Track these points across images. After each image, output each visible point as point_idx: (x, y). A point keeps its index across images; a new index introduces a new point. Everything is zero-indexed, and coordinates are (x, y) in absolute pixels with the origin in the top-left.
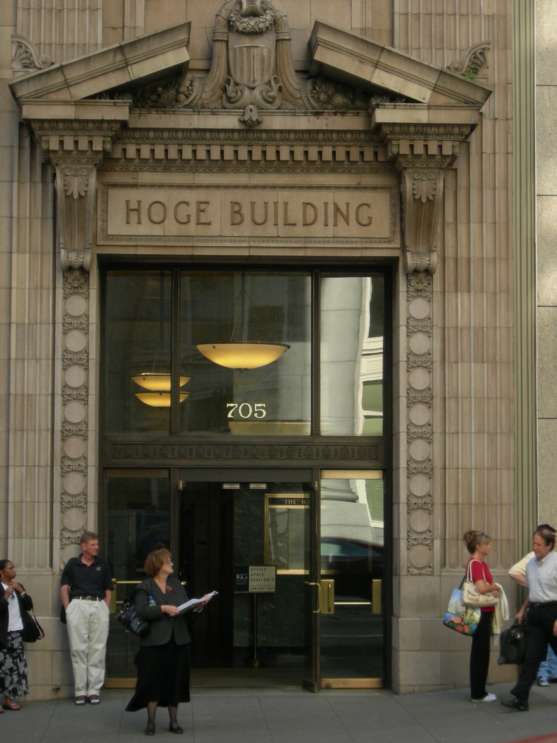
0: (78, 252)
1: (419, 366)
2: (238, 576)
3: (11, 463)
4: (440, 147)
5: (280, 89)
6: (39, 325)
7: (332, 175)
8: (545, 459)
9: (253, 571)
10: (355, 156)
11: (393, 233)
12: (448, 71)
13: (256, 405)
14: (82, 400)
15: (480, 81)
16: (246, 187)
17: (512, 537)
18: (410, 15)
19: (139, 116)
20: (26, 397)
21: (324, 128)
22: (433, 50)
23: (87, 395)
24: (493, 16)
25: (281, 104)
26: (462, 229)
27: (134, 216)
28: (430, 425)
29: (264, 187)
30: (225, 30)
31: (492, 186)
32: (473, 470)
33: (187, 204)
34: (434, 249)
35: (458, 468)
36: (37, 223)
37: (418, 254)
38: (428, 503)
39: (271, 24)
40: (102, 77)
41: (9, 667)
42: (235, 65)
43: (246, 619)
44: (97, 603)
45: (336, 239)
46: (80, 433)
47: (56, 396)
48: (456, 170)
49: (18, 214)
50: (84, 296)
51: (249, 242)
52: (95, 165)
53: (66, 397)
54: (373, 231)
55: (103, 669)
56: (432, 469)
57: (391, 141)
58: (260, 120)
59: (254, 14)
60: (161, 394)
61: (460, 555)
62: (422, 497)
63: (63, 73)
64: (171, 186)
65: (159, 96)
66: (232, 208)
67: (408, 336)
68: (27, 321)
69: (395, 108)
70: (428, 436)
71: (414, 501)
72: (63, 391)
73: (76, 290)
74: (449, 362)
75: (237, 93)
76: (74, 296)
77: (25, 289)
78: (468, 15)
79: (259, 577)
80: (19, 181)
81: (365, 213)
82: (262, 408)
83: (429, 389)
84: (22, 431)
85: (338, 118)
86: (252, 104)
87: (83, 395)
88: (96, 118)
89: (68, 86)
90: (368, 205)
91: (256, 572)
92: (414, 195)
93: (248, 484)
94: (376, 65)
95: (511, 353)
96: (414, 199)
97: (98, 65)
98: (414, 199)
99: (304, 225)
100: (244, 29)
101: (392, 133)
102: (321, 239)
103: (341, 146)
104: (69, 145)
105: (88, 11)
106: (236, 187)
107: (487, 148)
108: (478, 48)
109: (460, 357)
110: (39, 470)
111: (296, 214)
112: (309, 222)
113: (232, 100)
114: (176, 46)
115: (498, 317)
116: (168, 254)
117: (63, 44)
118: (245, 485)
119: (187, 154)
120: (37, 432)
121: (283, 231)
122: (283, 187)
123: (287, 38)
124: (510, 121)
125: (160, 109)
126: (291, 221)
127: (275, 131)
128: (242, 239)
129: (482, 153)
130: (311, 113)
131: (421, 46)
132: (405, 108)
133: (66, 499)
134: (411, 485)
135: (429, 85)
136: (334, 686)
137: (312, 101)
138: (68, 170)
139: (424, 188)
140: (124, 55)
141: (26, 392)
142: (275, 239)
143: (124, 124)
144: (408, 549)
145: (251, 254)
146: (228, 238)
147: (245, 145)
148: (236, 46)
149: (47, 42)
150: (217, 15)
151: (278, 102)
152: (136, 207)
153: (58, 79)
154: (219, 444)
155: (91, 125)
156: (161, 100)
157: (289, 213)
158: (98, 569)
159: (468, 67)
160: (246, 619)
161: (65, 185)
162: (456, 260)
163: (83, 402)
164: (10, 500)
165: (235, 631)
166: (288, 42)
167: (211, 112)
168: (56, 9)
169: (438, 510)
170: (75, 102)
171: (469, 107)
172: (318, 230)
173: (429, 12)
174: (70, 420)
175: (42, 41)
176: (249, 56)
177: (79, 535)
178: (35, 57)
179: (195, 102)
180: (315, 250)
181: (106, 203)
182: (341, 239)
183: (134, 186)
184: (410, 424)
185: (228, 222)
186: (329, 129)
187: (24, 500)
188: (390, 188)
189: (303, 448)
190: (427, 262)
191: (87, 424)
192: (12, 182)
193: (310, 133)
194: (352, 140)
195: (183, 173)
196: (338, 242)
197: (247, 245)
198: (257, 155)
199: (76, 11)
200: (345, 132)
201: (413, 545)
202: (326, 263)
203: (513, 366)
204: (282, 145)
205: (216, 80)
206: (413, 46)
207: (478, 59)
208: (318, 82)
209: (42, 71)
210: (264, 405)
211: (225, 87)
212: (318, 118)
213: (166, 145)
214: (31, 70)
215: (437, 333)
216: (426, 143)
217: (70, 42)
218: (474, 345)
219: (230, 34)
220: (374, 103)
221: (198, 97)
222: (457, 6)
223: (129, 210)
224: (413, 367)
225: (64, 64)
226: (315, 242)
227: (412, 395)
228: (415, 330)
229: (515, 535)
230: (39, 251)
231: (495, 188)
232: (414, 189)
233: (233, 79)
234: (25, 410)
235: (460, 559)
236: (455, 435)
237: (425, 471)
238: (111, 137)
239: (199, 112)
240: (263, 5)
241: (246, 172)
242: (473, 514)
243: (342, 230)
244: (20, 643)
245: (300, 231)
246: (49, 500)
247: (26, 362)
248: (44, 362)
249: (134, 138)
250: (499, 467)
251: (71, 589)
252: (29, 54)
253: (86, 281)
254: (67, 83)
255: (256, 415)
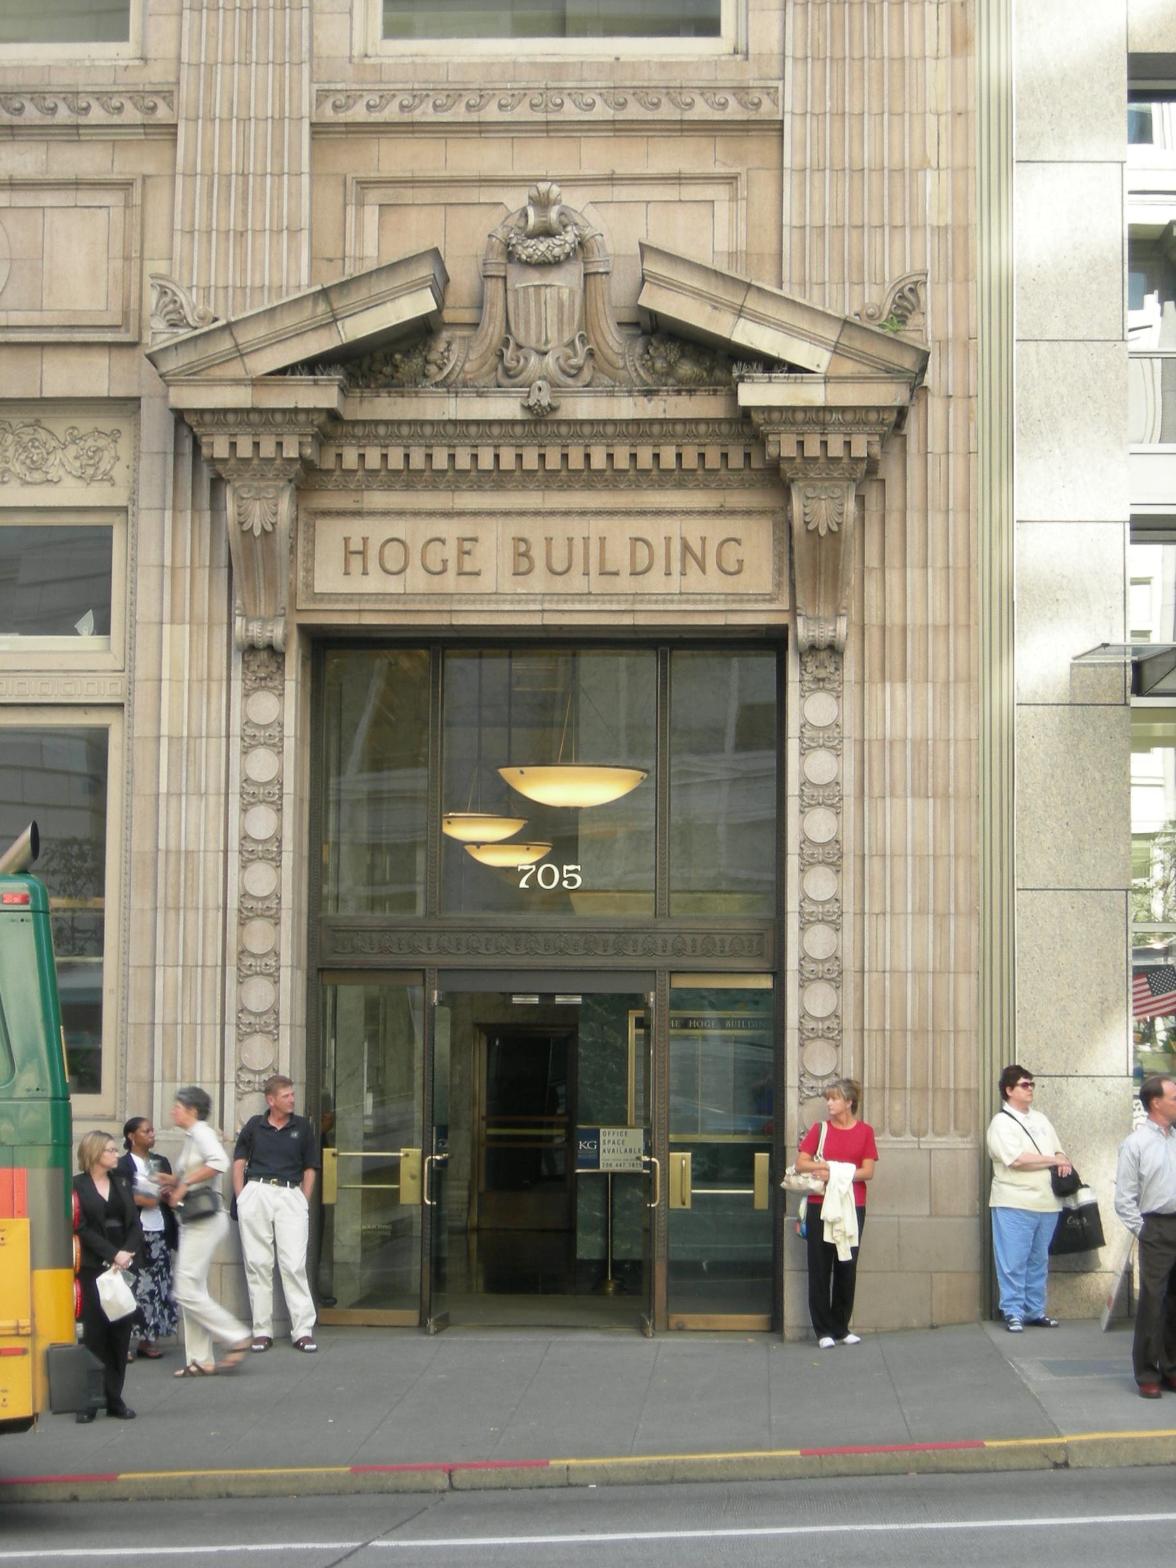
0: (265, 621)
1: (819, 804)
2: (581, 1145)
3: (159, 960)
4: (848, 444)
5: (591, 354)
6: (204, 740)
7: (676, 492)
8: (1029, 957)
9: (608, 1135)
10: (713, 460)
11: (778, 585)
12: (856, 320)
13: (565, 868)
14: (272, 859)
15: (909, 335)
16: (537, 513)
17: (973, 1085)
18: (808, 229)
19: (361, 402)
20: (183, 856)
21: (661, 416)
22: (847, 285)
23: (280, 853)
24: (946, 227)
25: (592, 378)
26: (893, 577)
27: (356, 563)
28: (837, 900)
29: (567, 513)
30: (502, 260)
31: (943, 508)
32: (909, 975)
33: (443, 541)
34: (843, 611)
35: (884, 972)
36: (203, 575)
37: (817, 619)
38: (834, 1029)
39: (574, 250)
40: (295, 340)
41: (147, 1290)
42: (517, 315)
43: (598, 1214)
44: (287, 1191)
45: (684, 597)
46: (268, 913)
47: (230, 854)
48: (883, 481)
49: (173, 561)
50: (277, 692)
51: (542, 602)
52: (290, 481)
53: (246, 855)
54: (746, 583)
55: (108, 1302)
56: (841, 973)
57: (767, 435)
58: (554, 405)
59: (547, 232)
60: (478, 847)
61: (887, 1114)
62: (823, 1019)
63: (232, 334)
64: (416, 514)
65: (396, 367)
66: (516, 547)
67: (802, 754)
68: (185, 734)
69: (770, 381)
70: (834, 918)
71: (811, 1024)
72: (242, 845)
73: (263, 683)
74: (871, 797)
75: (518, 362)
76: (260, 693)
77: (182, 681)
78: (903, 226)
79: (616, 1147)
80: (174, 508)
81: (732, 554)
82: (576, 871)
83: (837, 841)
84: (177, 909)
85: (683, 399)
86: (544, 378)
87: (272, 852)
88: (285, 406)
89: (242, 355)
90: (738, 541)
91: (611, 1138)
92: (807, 523)
93: (552, 996)
94: (740, 312)
95: (973, 780)
96: (808, 531)
97: (289, 321)
98: (808, 531)
99: (631, 574)
100: (530, 257)
101: (768, 422)
102: (660, 597)
103: (690, 444)
104: (813, 448)
105: (285, 232)
106: (522, 513)
107: (935, 444)
108: (907, 281)
109: (888, 789)
110: (203, 972)
111: (619, 556)
112: (639, 569)
113: (512, 373)
114: (413, 287)
115: (952, 723)
116: (488, 623)
117: (246, 287)
118: (547, 996)
119: (441, 460)
120: (201, 912)
121: (597, 584)
122: (598, 513)
123: (601, 270)
124: (973, 400)
125: (393, 390)
126: (610, 567)
127: (582, 422)
128: (533, 597)
129: (927, 453)
130: (638, 391)
131: (827, 279)
132: (787, 381)
133: (246, 1019)
134: (806, 999)
135: (827, 344)
136: (691, 1326)
137: (642, 373)
138: (245, 489)
139: (823, 511)
140: (330, 304)
141: (183, 848)
142: (585, 597)
143: (333, 415)
144: (801, 1104)
145: (545, 622)
146: (509, 597)
147: (534, 445)
148: (518, 286)
149: (221, 284)
150: (490, 236)
151: (586, 375)
152: (361, 549)
153: (225, 344)
154: (501, 931)
155: (279, 418)
156: (398, 375)
157: (608, 555)
158: (295, 1135)
159: (890, 312)
160: (598, 1214)
161: (239, 514)
162: (883, 628)
163: (274, 864)
164: (156, 1021)
165: (579, 1235)
166: (604, 277)
167: (477, 392)
168: (235, 231)
169: (849, 1040)
170: (252, 380)
171: (892, 378)
172: (655, 582)
173: (840, 224)
174: (252, 893)
175: (213, 283)
176: (538, 301)
177: (265, 1077)
178: (187, 310)
179: (453, 377)
180: (649, 614)
181: (311, 541)
182: (692, 597)
183: (358, 514)
184: (805, 898)
185: (508, 569)
186: (668, 417)
187: (179, 1021)
188: (773, 512)
189: (641, 938)
190: (832, 634)
191: (280, 899)
192: (164, 509)
193: (638, 425)
194: (707, 435)
195: (436, 493)
196: (687, 602)
197: (539, 607)
198: (553, 462)
199: (267, 233)
200: (697, 421)
201: (809, 1097)
202: (677, 636)
203: (978, 803)
204: (593, 444)
205: (487, 341)
206: (814, 280)
207: (907, 299)
208: (653, 340)
209: (197, 332)
210: (579, 867)
211: (501, 351)
212: (650, 401)
213: (407, 447)
214: (181, 331)
215: (849, 749)
216: (824, 439)
217: (258, 284)
218: (913, 769)
219: (509, 265)
220: (735, 374)
221: (458, 369)
222: (886, 213)
223: (349, 553)
224: (810, 806)
225: (233, 319)
226: (649, 602)
227: (807, 851)
228: (813, 744)
229: (978, 1081)
230: (206, 621)
231: (947, 511)
232: (805, 514)
233: (514, 339)
234: (182, 877)
235: (887, 1120)
236: (881, 916)
237: (828, 976)
238: (312, 436)
239: (457, 393)
240: (563, 218)
241: (538, 488)
242: (909, 1047)
243: (695, 581)
244: (161, 1249)
245: (625, 583)
246: (218, 1021)
247: (184, 798)
248: (212, 799)
249: (354, 436)
250: (952, 970)
251: (249, 1166)
252: (178, 305)
253: (278, 668)
254: (239, 351)
255: (565, 884)
